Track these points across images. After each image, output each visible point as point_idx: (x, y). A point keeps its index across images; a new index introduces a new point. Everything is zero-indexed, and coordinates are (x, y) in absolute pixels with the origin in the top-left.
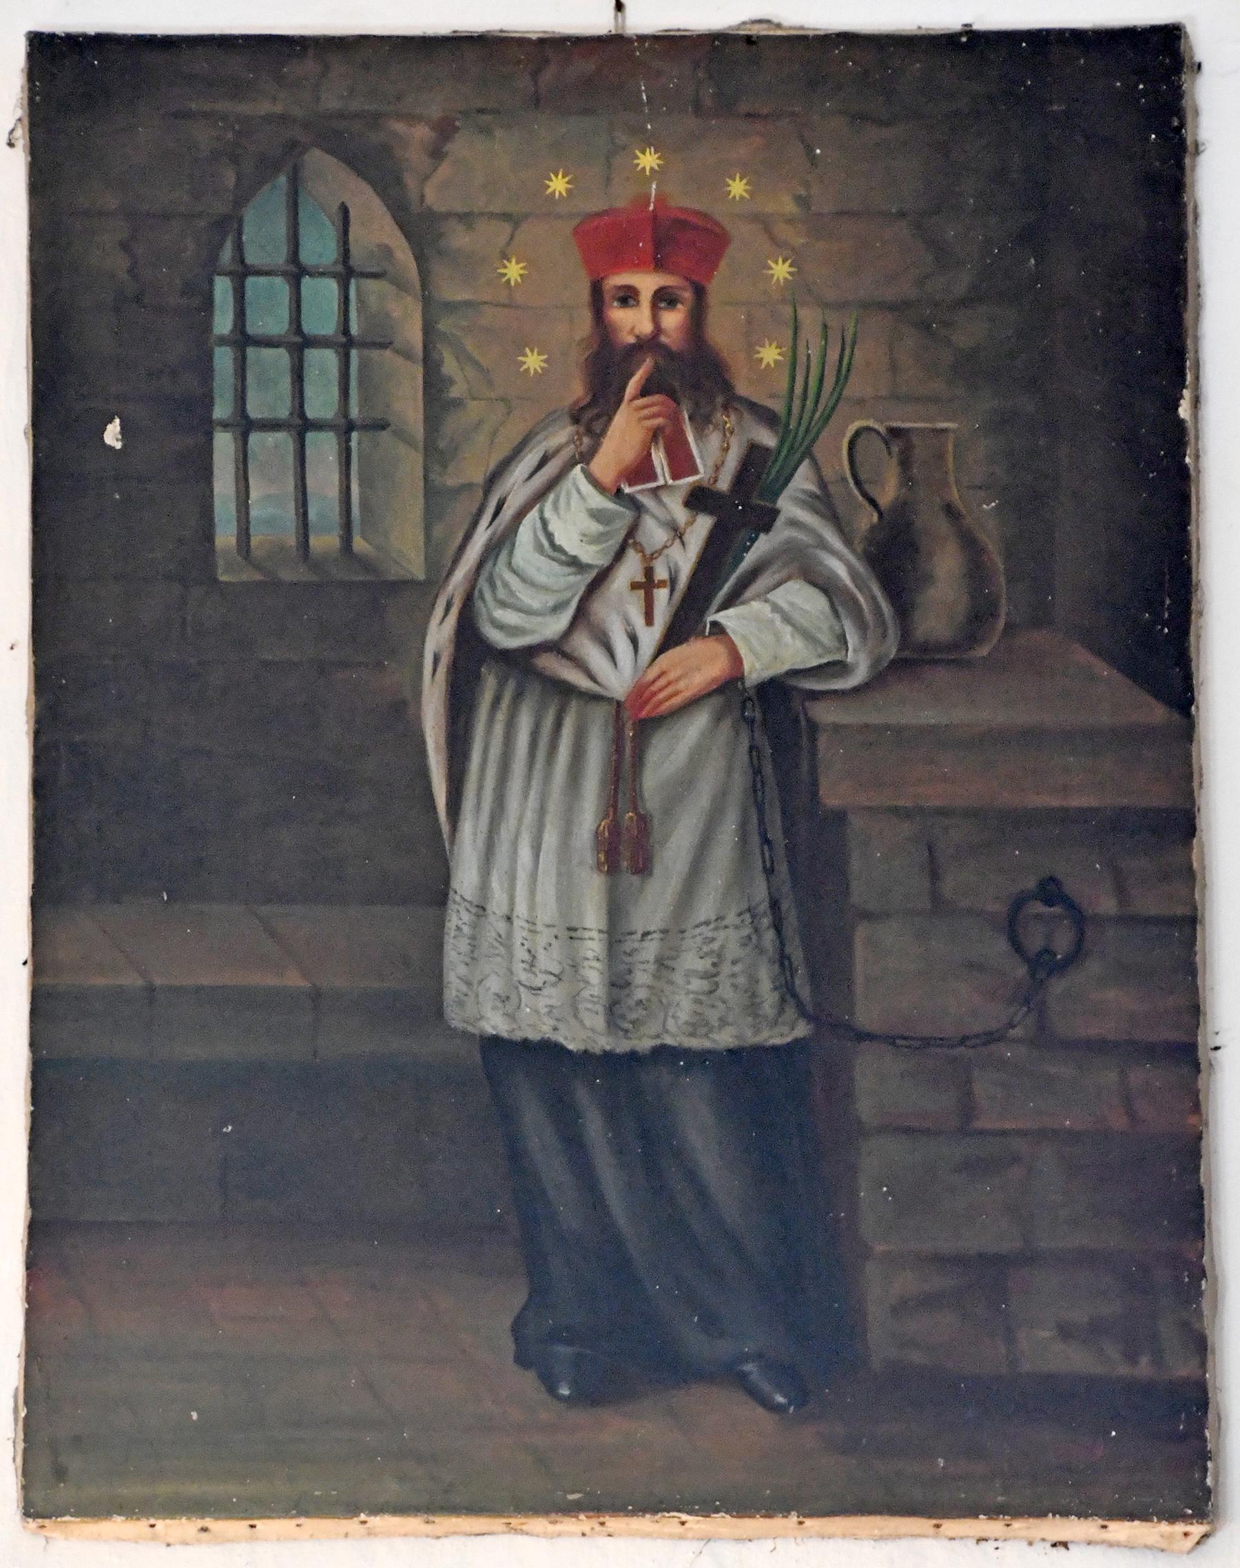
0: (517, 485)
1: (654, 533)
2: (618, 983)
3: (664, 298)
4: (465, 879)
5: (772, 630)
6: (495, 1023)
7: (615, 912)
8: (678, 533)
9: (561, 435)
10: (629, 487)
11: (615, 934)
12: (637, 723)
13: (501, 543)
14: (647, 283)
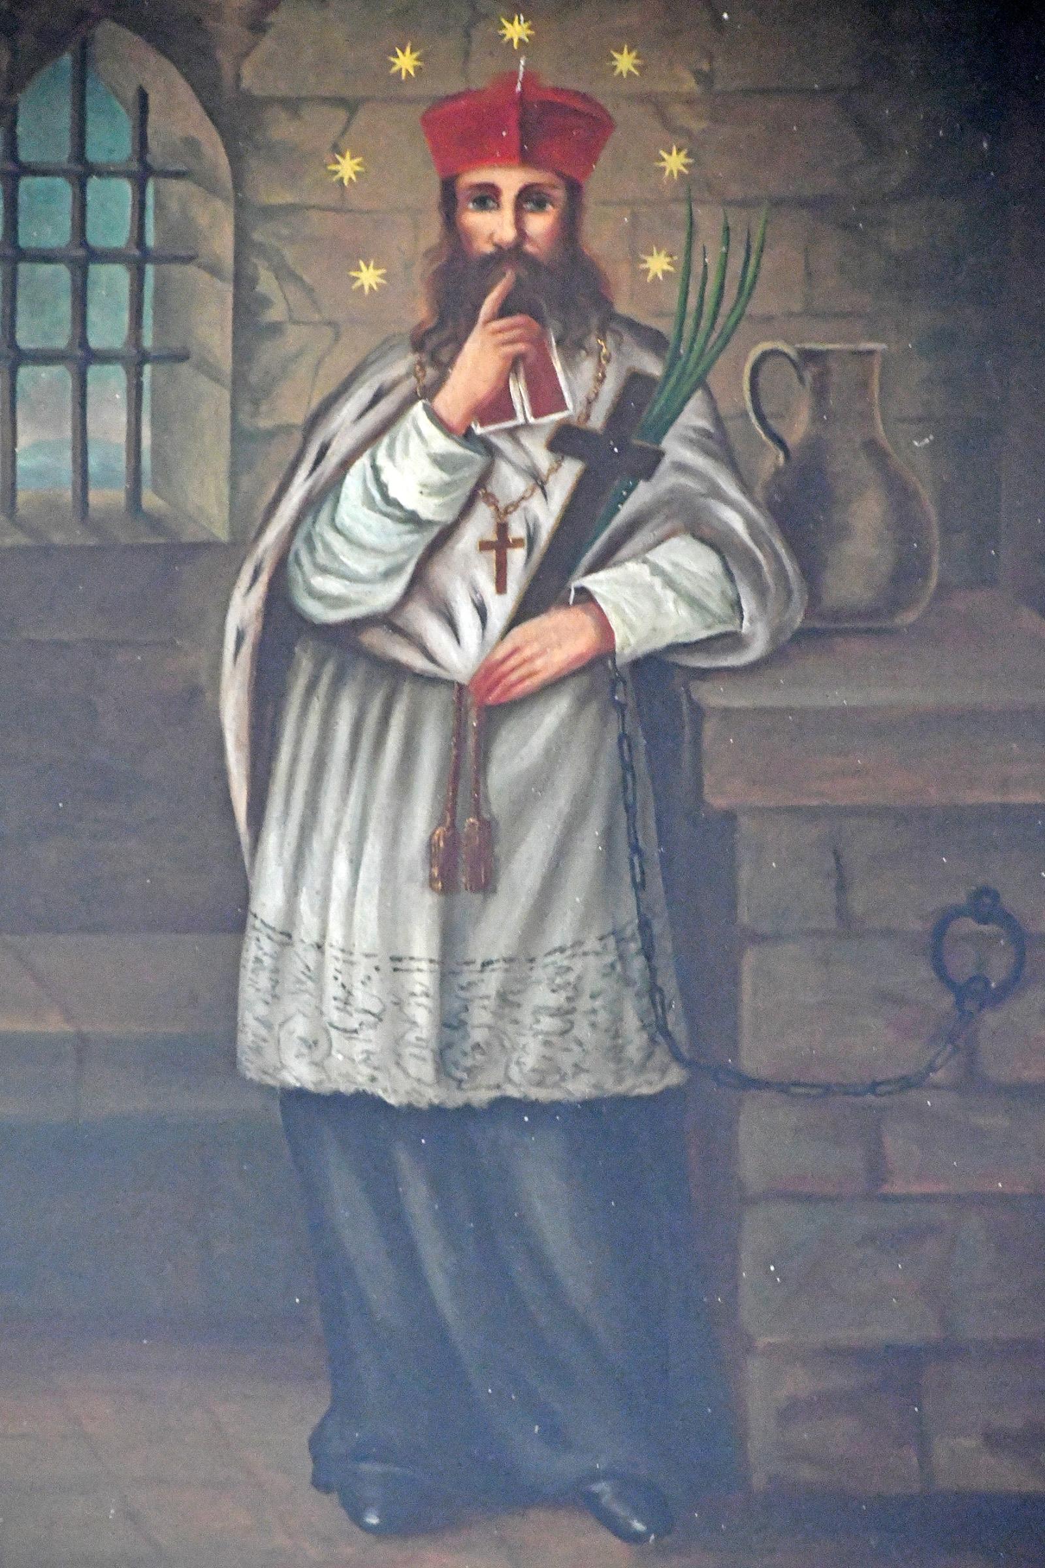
0: (345, 425)
1: (510, 483)
2: (451, 1024)
3: (530, 199)
4: (268, 901)
5: (649, 597)
6: (299, 1072)
7: (451, 937)
8: (539, 482)
9: (400, 366)
12: (483, 709)
13: (324, 496)
14: (511, 181)
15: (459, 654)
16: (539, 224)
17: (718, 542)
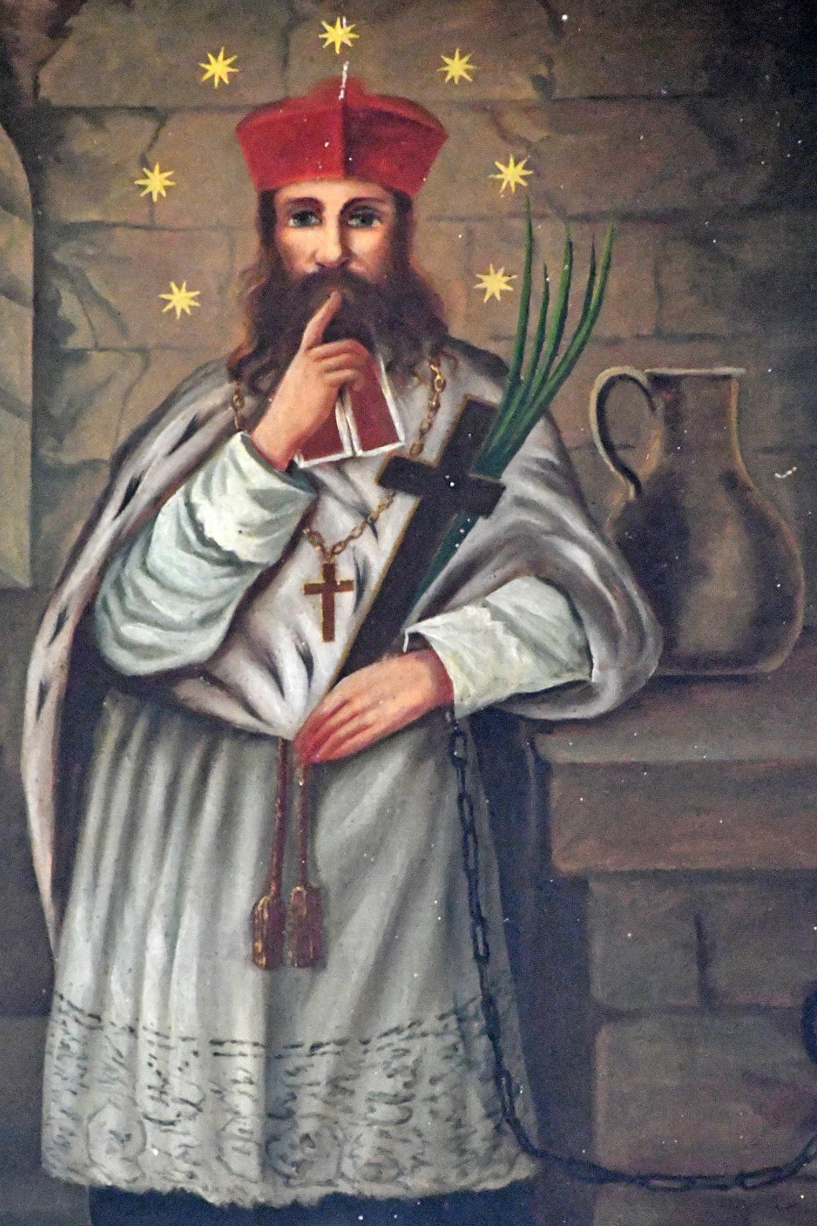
0: (156, 460)
1: (337, 520)
2: (278, 1114)
3: (355, 214)
4: (76, 979)
5: (491, 643)
6: (110, 1170)
7: (276, 1017)
8: (369, 520)
9: (215, 395)
10: (304, 463)
11: (275, 1049)
12: (310, 767)
14: (333, 194)
15: (284, 708)
16: (367, 242)
17: (564, 583)
